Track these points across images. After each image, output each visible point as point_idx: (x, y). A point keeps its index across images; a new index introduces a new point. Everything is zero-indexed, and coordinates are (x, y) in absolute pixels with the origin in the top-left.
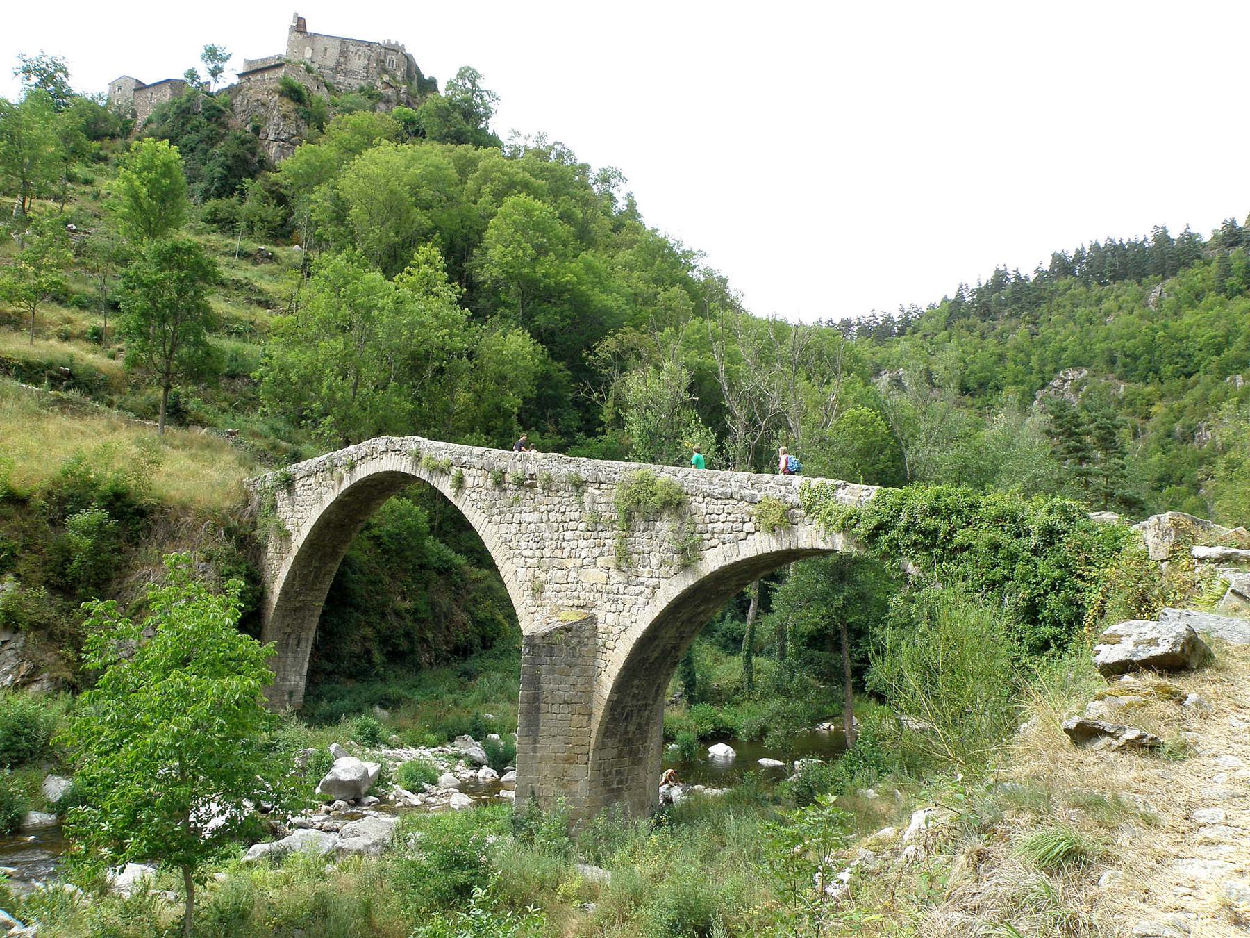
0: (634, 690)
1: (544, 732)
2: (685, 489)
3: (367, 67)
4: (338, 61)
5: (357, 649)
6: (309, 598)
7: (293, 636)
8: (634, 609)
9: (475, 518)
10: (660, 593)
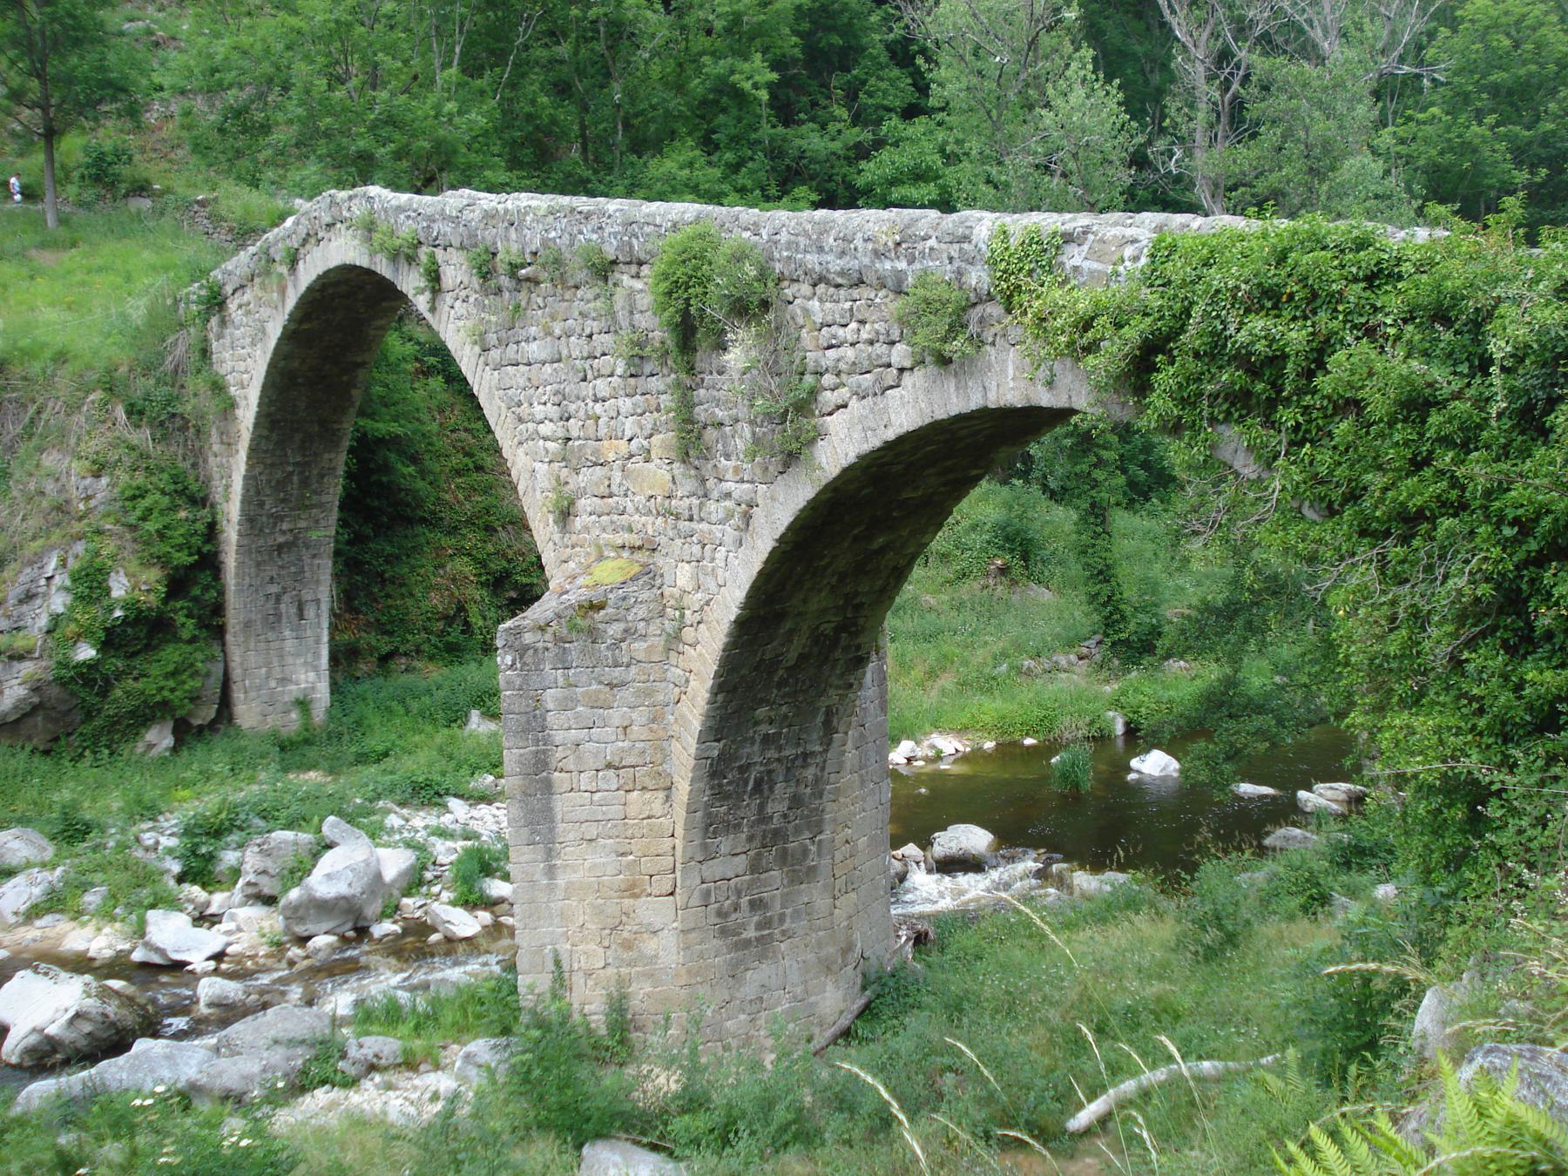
2: (778, 267)
5: (436, 601)
6: (302, 524)
7: (286, 598)
9: (467, 359)
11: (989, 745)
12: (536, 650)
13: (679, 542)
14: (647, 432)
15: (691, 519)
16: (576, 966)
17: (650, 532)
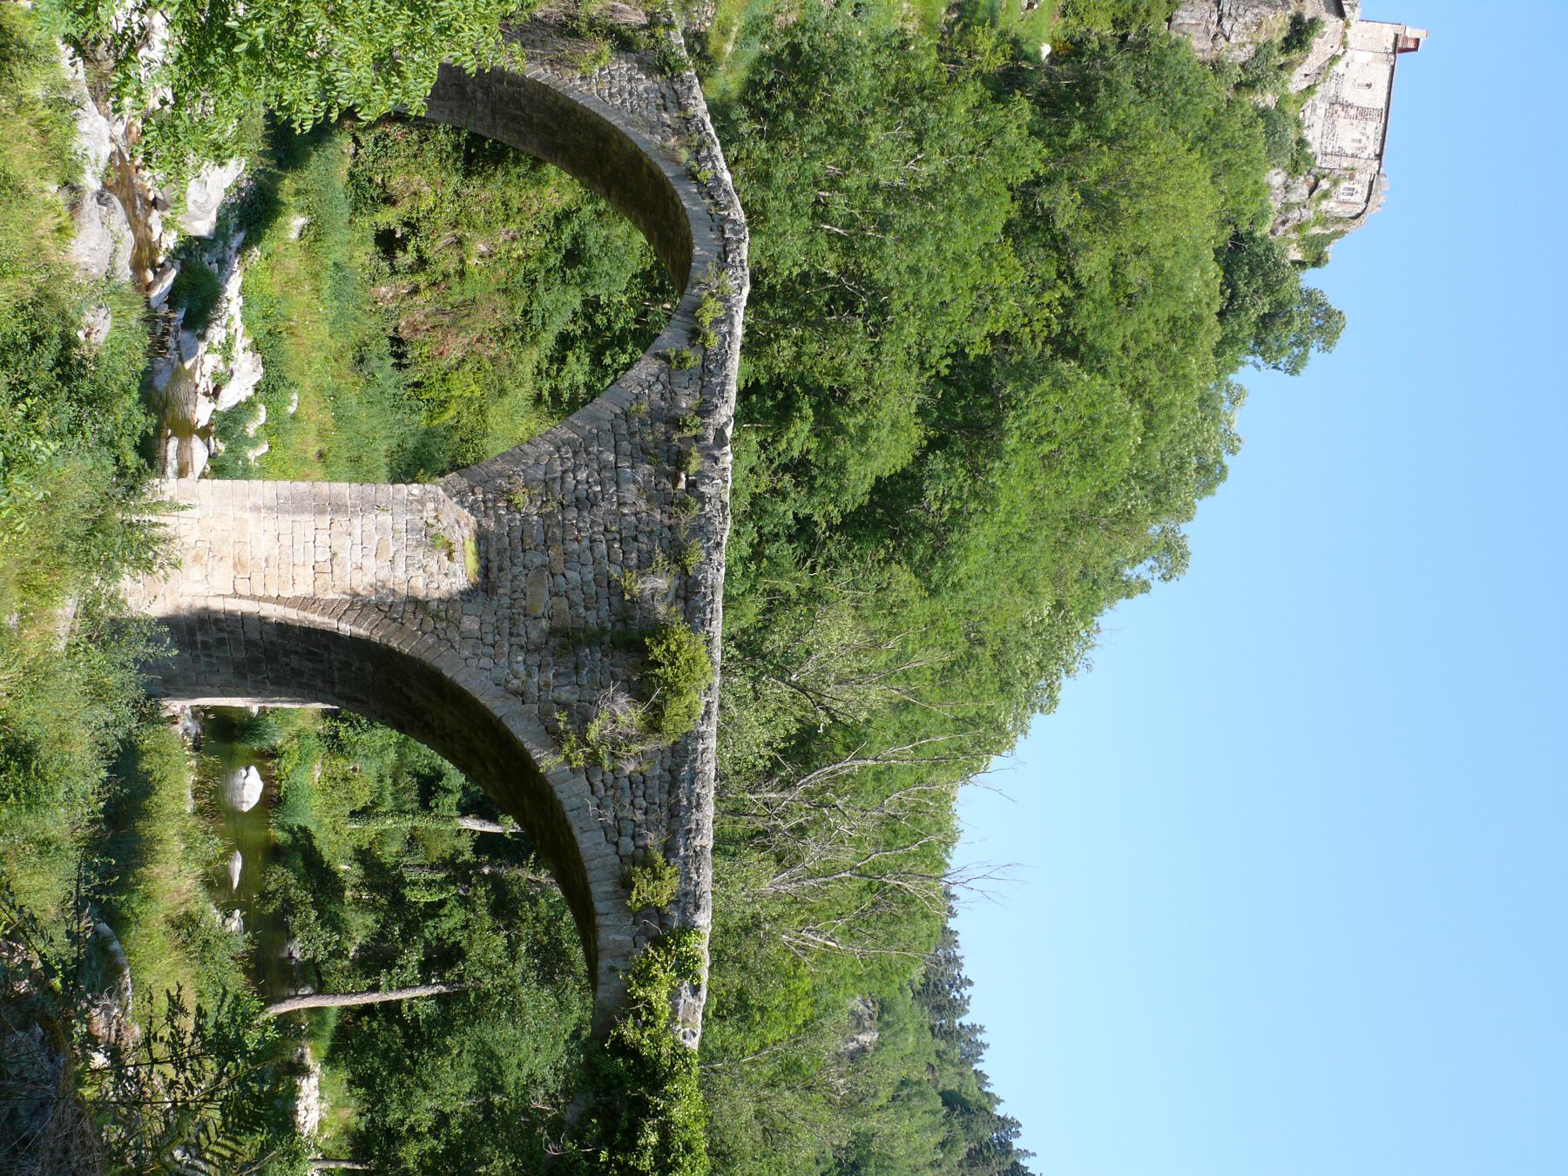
0: (356, 665)
1: (285, 522)
3: (1340, 154)
4: (1350, 106)
6: (480, 108)
8: (485, 662)
10: (515, 704)
12: (421, 511)
15: (511, 634)
16: (182, 521)
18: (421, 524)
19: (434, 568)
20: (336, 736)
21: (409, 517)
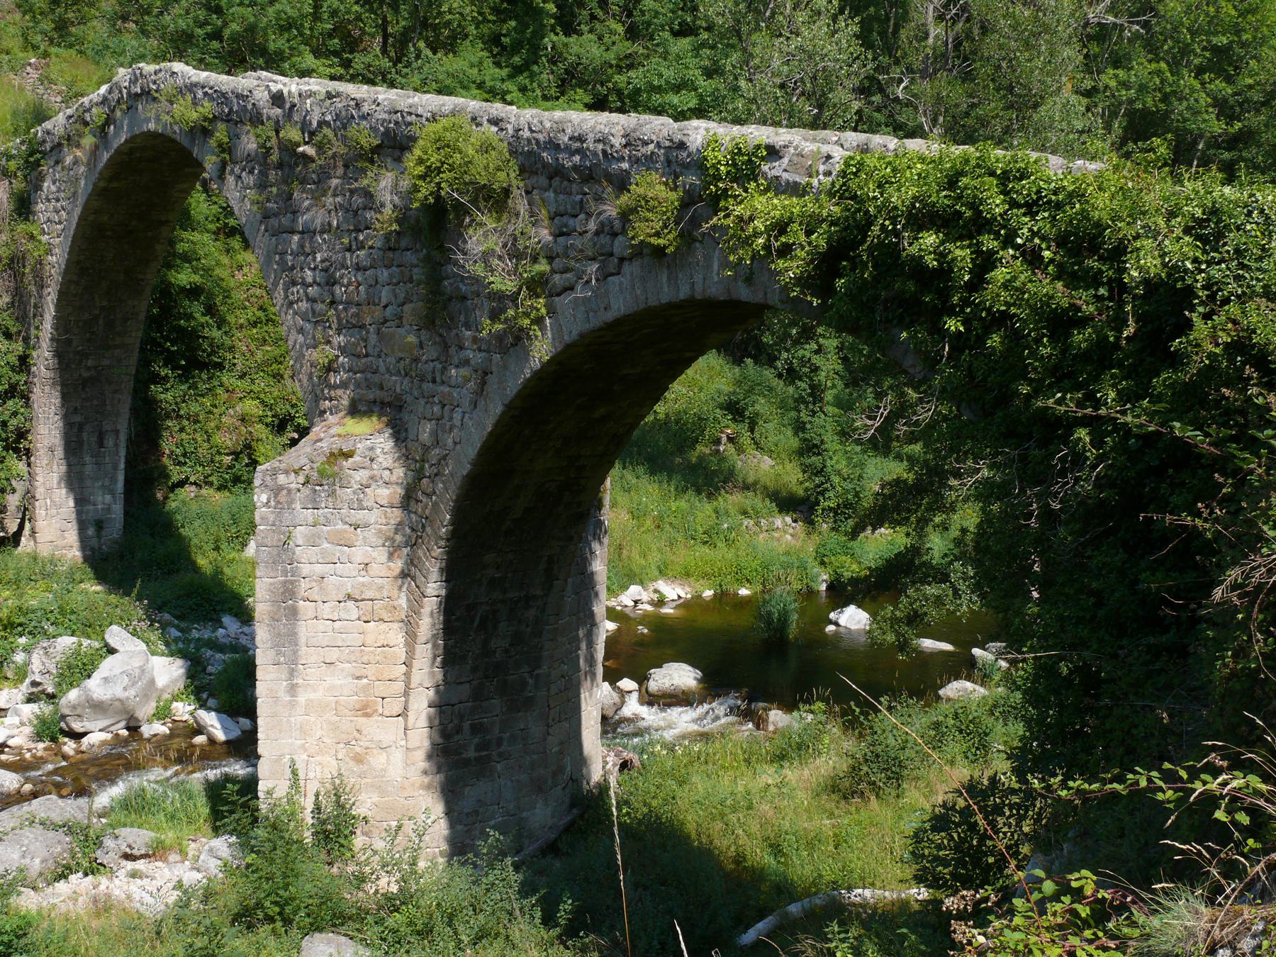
6: (106, 362)
7: (88, 428)
11: (708, 593)
12: (289, 491)
13: (422, 401)
14: (401, 299)
16: (311, 775)
17: (398, 390)
18: (306, 491)
19: (361, 476)
20: (835, 511)
21: (298, 506)
